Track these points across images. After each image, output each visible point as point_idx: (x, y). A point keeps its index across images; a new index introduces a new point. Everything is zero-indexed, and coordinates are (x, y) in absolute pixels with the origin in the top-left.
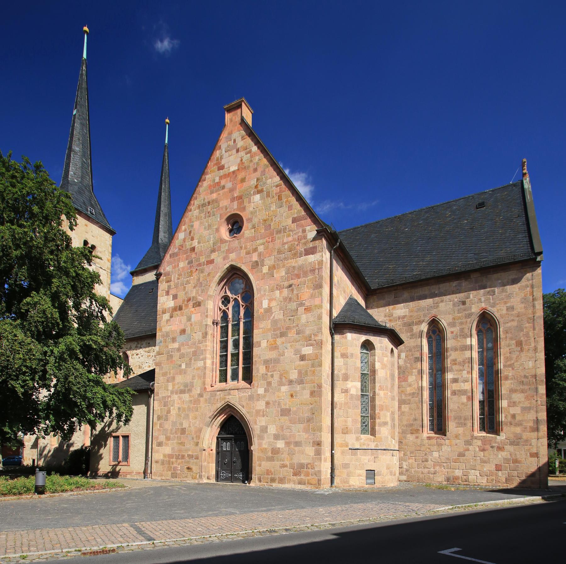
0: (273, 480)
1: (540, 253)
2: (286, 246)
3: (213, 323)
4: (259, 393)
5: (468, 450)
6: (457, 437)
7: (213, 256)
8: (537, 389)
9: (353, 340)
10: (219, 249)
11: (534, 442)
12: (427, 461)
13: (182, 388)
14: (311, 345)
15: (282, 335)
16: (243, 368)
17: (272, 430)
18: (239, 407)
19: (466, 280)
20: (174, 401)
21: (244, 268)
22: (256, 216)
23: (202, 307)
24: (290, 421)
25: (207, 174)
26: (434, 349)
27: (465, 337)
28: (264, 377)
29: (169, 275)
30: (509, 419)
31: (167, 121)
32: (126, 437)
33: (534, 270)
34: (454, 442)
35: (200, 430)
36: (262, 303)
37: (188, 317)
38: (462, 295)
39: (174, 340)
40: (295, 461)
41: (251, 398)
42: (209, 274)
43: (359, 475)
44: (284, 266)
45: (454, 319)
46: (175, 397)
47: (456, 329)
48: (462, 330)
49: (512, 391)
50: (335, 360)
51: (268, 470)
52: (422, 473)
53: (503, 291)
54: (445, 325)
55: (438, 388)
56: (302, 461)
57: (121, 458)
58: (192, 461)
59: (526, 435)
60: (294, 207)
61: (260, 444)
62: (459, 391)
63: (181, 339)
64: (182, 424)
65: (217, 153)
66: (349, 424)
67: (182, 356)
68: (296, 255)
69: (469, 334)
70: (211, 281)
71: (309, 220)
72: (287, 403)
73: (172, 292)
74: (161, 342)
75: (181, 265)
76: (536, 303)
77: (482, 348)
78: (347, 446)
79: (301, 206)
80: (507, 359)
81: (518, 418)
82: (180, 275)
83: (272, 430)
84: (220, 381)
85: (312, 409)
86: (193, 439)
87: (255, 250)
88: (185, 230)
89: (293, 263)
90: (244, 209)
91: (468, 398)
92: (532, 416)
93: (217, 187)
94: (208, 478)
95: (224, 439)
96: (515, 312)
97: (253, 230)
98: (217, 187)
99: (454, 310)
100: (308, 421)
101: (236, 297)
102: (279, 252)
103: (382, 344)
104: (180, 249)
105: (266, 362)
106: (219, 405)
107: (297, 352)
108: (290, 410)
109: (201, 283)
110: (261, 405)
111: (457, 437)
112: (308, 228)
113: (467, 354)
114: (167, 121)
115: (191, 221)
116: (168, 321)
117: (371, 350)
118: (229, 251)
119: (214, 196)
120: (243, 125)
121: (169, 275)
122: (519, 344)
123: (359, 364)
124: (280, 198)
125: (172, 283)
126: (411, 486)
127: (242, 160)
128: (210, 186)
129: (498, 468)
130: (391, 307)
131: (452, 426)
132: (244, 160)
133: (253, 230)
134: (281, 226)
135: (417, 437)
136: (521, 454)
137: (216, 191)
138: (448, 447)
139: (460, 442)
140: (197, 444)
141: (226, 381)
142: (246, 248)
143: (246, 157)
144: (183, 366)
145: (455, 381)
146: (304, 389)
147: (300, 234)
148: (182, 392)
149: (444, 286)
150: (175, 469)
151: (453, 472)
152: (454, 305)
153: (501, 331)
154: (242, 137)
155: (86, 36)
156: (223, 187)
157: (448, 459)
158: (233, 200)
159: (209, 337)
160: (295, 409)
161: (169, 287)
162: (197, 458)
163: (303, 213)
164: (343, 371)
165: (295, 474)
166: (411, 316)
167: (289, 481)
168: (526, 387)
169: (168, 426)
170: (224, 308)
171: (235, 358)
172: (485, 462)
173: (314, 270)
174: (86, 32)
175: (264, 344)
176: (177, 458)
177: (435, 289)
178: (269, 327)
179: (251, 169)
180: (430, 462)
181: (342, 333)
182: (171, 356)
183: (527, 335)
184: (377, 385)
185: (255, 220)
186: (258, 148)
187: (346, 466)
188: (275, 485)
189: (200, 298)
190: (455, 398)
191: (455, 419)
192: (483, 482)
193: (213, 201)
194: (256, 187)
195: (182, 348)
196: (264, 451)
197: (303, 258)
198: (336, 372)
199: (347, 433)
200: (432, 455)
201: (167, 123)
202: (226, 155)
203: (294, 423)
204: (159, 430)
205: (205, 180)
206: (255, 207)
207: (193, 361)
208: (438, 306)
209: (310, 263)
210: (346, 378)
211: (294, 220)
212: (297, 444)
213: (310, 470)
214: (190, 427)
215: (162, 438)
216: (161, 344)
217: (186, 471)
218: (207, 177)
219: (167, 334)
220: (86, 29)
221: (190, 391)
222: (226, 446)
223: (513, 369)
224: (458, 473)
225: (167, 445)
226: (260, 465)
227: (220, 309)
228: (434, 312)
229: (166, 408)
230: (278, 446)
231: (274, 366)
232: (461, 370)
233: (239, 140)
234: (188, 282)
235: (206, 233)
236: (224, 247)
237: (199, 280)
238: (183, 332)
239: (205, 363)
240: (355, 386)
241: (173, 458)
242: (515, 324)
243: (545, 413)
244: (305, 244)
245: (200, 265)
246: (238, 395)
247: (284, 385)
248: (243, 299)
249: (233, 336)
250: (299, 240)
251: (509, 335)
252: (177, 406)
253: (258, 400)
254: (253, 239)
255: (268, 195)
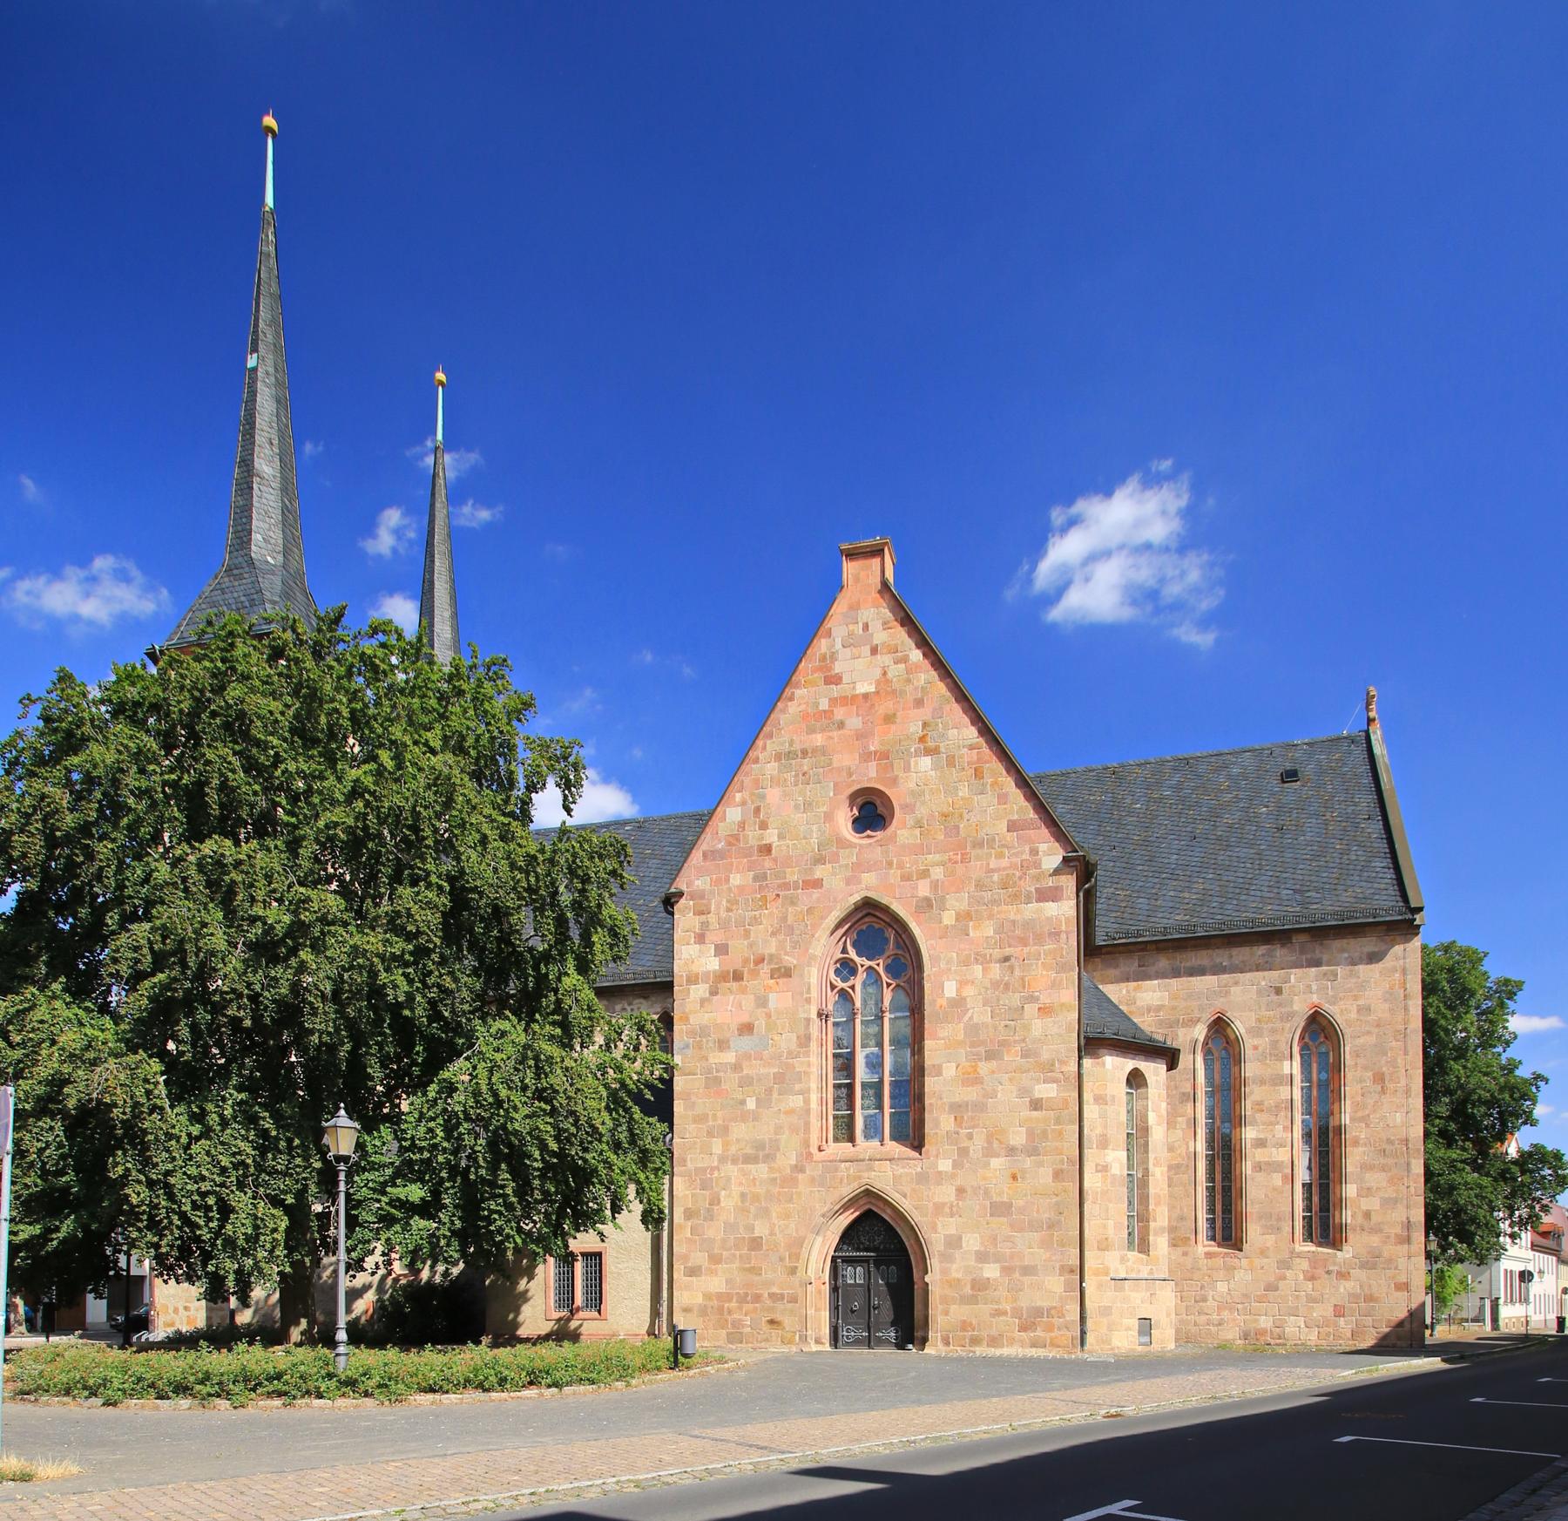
0: (975, 1341)
1: (1420, 909)
2: (996, 877)
3: (820, 1015)
4: (940, 1168)
5: (1284, 1278)
6: (1263, 1252)
7: (820, 872)
8: (1408, 1164)
9: (1115, 1066)
10: (835, 859)
11: (1402, 1263)
12: (1204, 1300)
13: (749, 1151)
14: (1054, 1081)
15: (990, 1056)
16: (892, 1115)
17: (972, 1242)
18: (894, 1196)
19: (1283, 945)
20: (729, 1179)
21: (896, 907)
22: (924, 803)
23: (795, 980)
24: (1012, 1226)
25: (797, 686)
26: (1217, 1076)
27: (1280, 1058)
28: (952, 1137)
29: (702, 897)
30: (1360, 1219)
31: (441, 376)
32: (595, 1258)
33: (1408, 941)
34: (1258, 1262)
35: (800, 1242)
36: (943, 983)
37: (757, 998)
38: (1275, 974)
39: (722, 1045)
40: (1024, 1303)
41: (922, 1178)
42: (810, 911)
43: (1128, 1329)
44: (990, 917)
45: (1259, 1020)
46: (732, 1170)
47: (1264, 1042)
48: (1274, 1044)
49: (1366, 1167)
50: (1086, 1107)
51: (964, 1322)
52: (1196, 1324)
53: (1351, 974)
54: (1243, 1031)
55: (1224, 1157)
56: (1039, 1304)
57: (579, 1299)
58: (779, 1306)
59: (1389, 1250)
60: (1011, 798)
61: (944, 1272)
62: (1268, 1164)
63: (745, 1043)
64: (751, 1228)
65: (821, 646)
66: (1111, 1232)
67: (746, 1082)
68: (1015, 898)
69: (1287, 1053)
70: (815, 926)
71: (1045, 832)
72: (1003, 1191)
73: (714, 937)
74: (687, 1046)
75: (736, 880)
76: (1410, 1003)
77: (1309, 1081)
78: (1107, 1274)
79: (1027, 799)
80: (1357, 1106)
81: (1375, 1218)
82: (733, 902)
83: (972, 1242)
84: (836, 1140)
85: (1057, 1204)
86: (781, 1259)
87: (925, 874)
88: (744, 803)
89: (1011, 912)
90: (894, 781)
91: (1284, 1177)
92: (1399, 1215)
93: (822, 719)
94: (818, 1342)
95: (849, 1261)
96: (1373, 1017)
97: (917, 831)
98: (822, 719)
99: (1263, 1004)
100: (1050, 1227)
101: (872, 963)
102: (980, 886)
103: (1154, 1071)
104: (730, 844)
105: (957, 1109)
106: (848, 1190)
107: (1024, 1092)
108: (1011, 1205)
109: (791, 928)
110: (946, 1193)
111: (1263, 1252)
112: (1043, 847)
113: (1284, 1092)
114: (441, 376)
115: (757, 783)
116: (703, 1001)
117: (1138, 1087)
118: (859, 867)
119: (819, 739)
120: (887, 596)
121: (702, 897)
122: (1379, 1078)
123: (1123, 1117)
124: (978, 774)
125: (712, 918)
126: (1190, 1350)
127: (885, 674)
128: (805, 716)
129: (1339, 1312)
130: (1132, 985)
131: (1254, 1232)
132: (890, 675)
133: (917, 831)
134: (982, 834)
135: (1185, 1254)
136: (1380, 1284)
137: (823, 731)
138: (1239, 1276)
139: (1270, 1263)
140: (793, 1271)
141: (851, 1139)
142: (901, 866)
143: (896, 671)
144: (751, 1104)
145: (1261, 1143)
146: (1040, 1164)
147: (1026, 856)
148: (749, 1159)
149: (1241, 954)
150: (737, 1324)
151: (1256, 1321)
152: (1259, 992)
153: (1348, 1050)
154: (884, 623)
155: (270, 141)
156: (841, 725)
157: (1246, 1296)
158: (867, 756)
159: (814, 1046)
160: (1021, 1203)
161: (705, 925)
162: (794, 1300)
163: (1032, 814)
164: (1098, 1131)
165: (1023, 1329)
166: (1174, 1008)
167: (1012, 1342)
168: (1391, 1161)
169: (714, 1231)
170: (840, 984)
171: (871, 1092)
172: (1315, 1301)
173: (1058, 934)
174: (269, 130)
175: (949, 1070)
176: (743, 1300)
177: (1221, 956)
178: (961, 1037)
179: (910, 698)
180: (1210, 1302)
181: (1095, 1055)
182: (718, 1081)
183: (1393, 1063)
184: (1151, 1156)
185: (922, 811)
186: (925, 655)
187: (1106, 1311)
188: (980, 1351)
189: (790, 960)
190: (1260, 1177)
191: (1260, 1218)
192: (1312, 1337)
193: (815, 750)
194: (922, 739)
195: (745, 1064)
196: (955, 1284)
197: (1034, 905)
198: (1086, 1131)
199: (1106, 1249)
200: (1214, 1289)
201: (441, 383)
202: (844, 654)
203: (1021, 1230)
204: (689, 1241)
205: (791, 699)
206: (916, 783)
207: (775, 1095)
208: (1227, 993)
209: (1049, 919)
210: (1104, 1143)
211: (1012, 827)
212: (1028, 1270)
213: (1056, 1321)
214: (772, 1234)
215: (700, 1258)
216: (689, 1052)
217: (765, 1327)
218: (798, 692)
219: (704, 1031)
220: (269, 121)
221: (769, 1158)
222: (854, 1276)
223: (1367, 1126)
224: (1265, 1322)
225: (713, 1272)
226: (946, 1313)
227: (833, 987)
228: (1220, 1004)
229: (707, 1193)
230: (986, 1274)
231: (973, 1118)
232: (1271, 1124)
233: (876, 626)
234: (756, 921)
235: (799, 818)
236: (848, 858)
237: (784, 919)
238: (747, 1029)
239: (807, 1102)
240: (1117, 1158)
241: (730, 1301)
242: (1372, 1039)
243: (1422, 1210)
244: (1037, 878)
245: (786, 886)
246: (890, 1171)
247: (998, 1156)
248: (888, 969)
249: (863, 1046)
250: (1024, 867)
251: (1361, 1061)
252: (736, 1190)
253: (939, 1183)
254: (919, 850)
255: (951, 761)
